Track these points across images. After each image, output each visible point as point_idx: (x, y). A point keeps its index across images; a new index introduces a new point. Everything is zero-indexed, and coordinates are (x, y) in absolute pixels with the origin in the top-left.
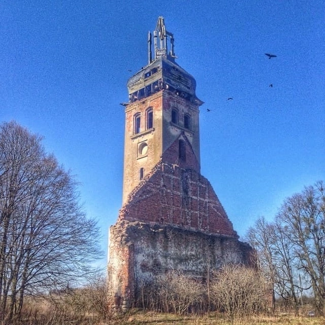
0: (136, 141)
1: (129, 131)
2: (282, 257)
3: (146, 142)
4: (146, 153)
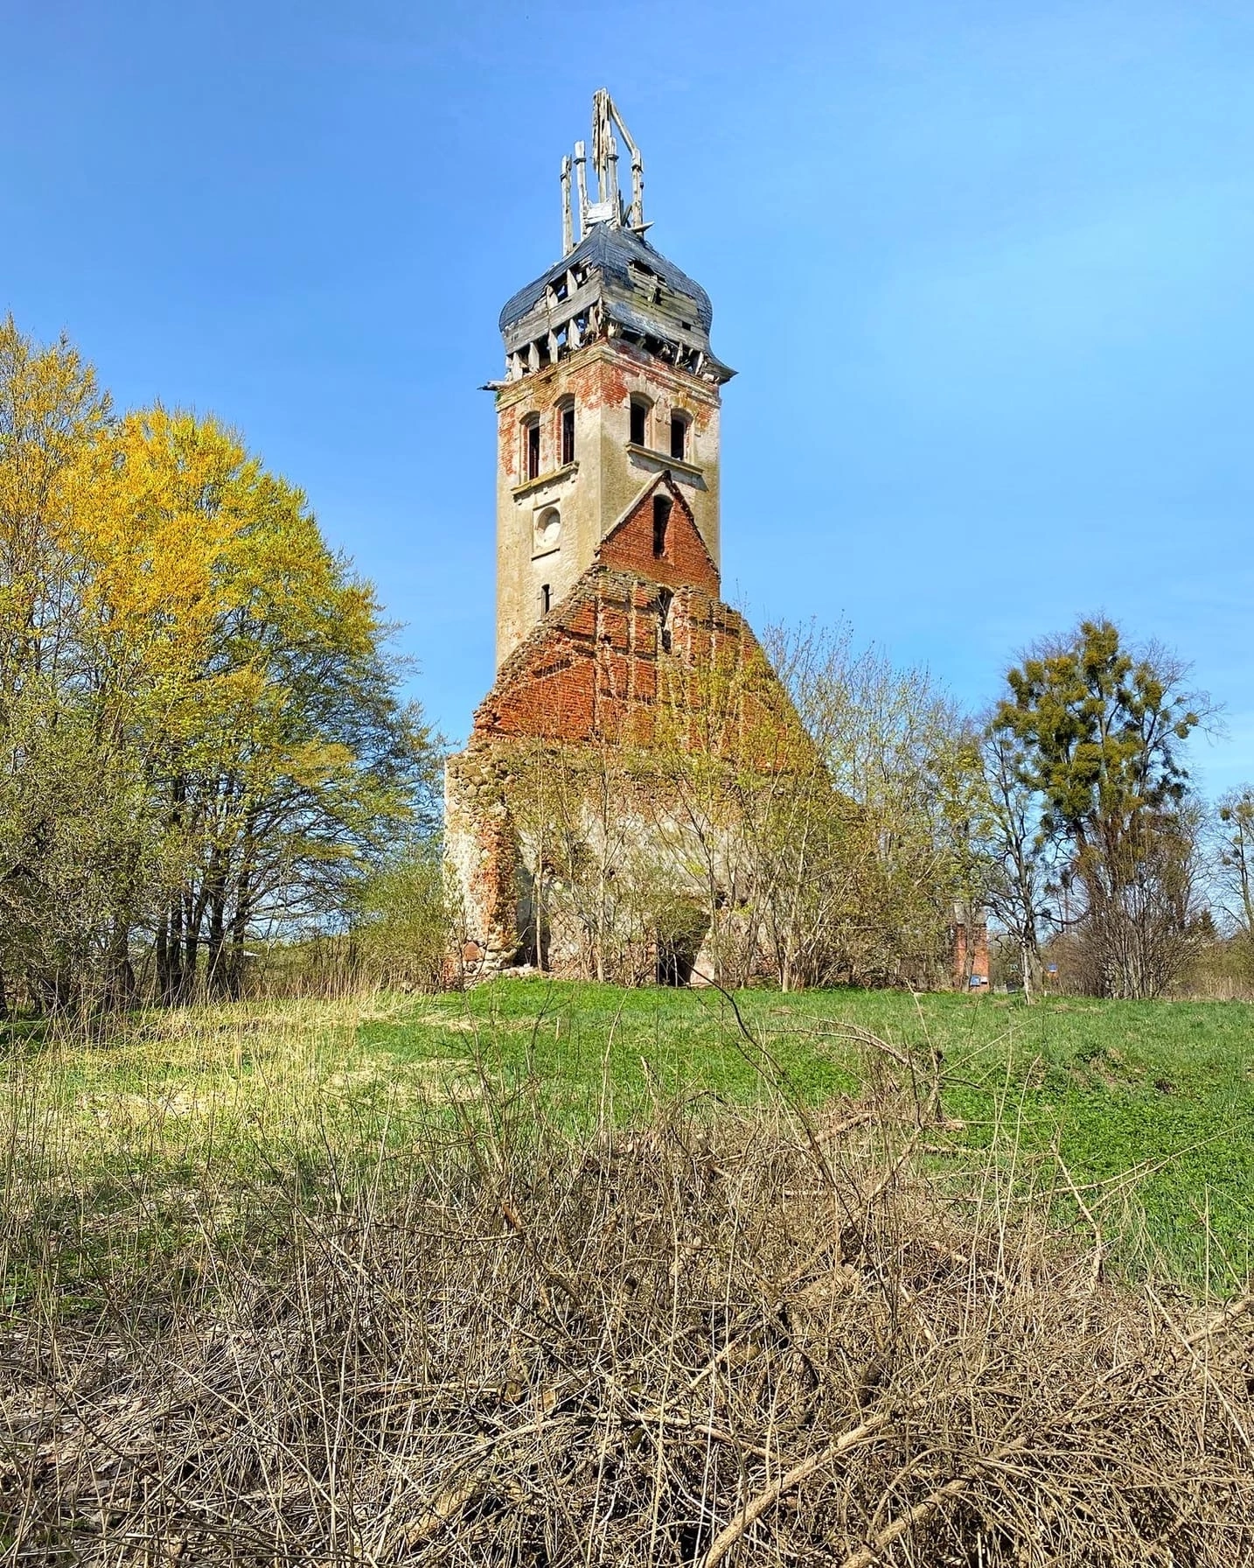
0: (528, 503)
1: (510, 471)
2: (1004, 833)
3: (557, 506)
4: (555, 542)
